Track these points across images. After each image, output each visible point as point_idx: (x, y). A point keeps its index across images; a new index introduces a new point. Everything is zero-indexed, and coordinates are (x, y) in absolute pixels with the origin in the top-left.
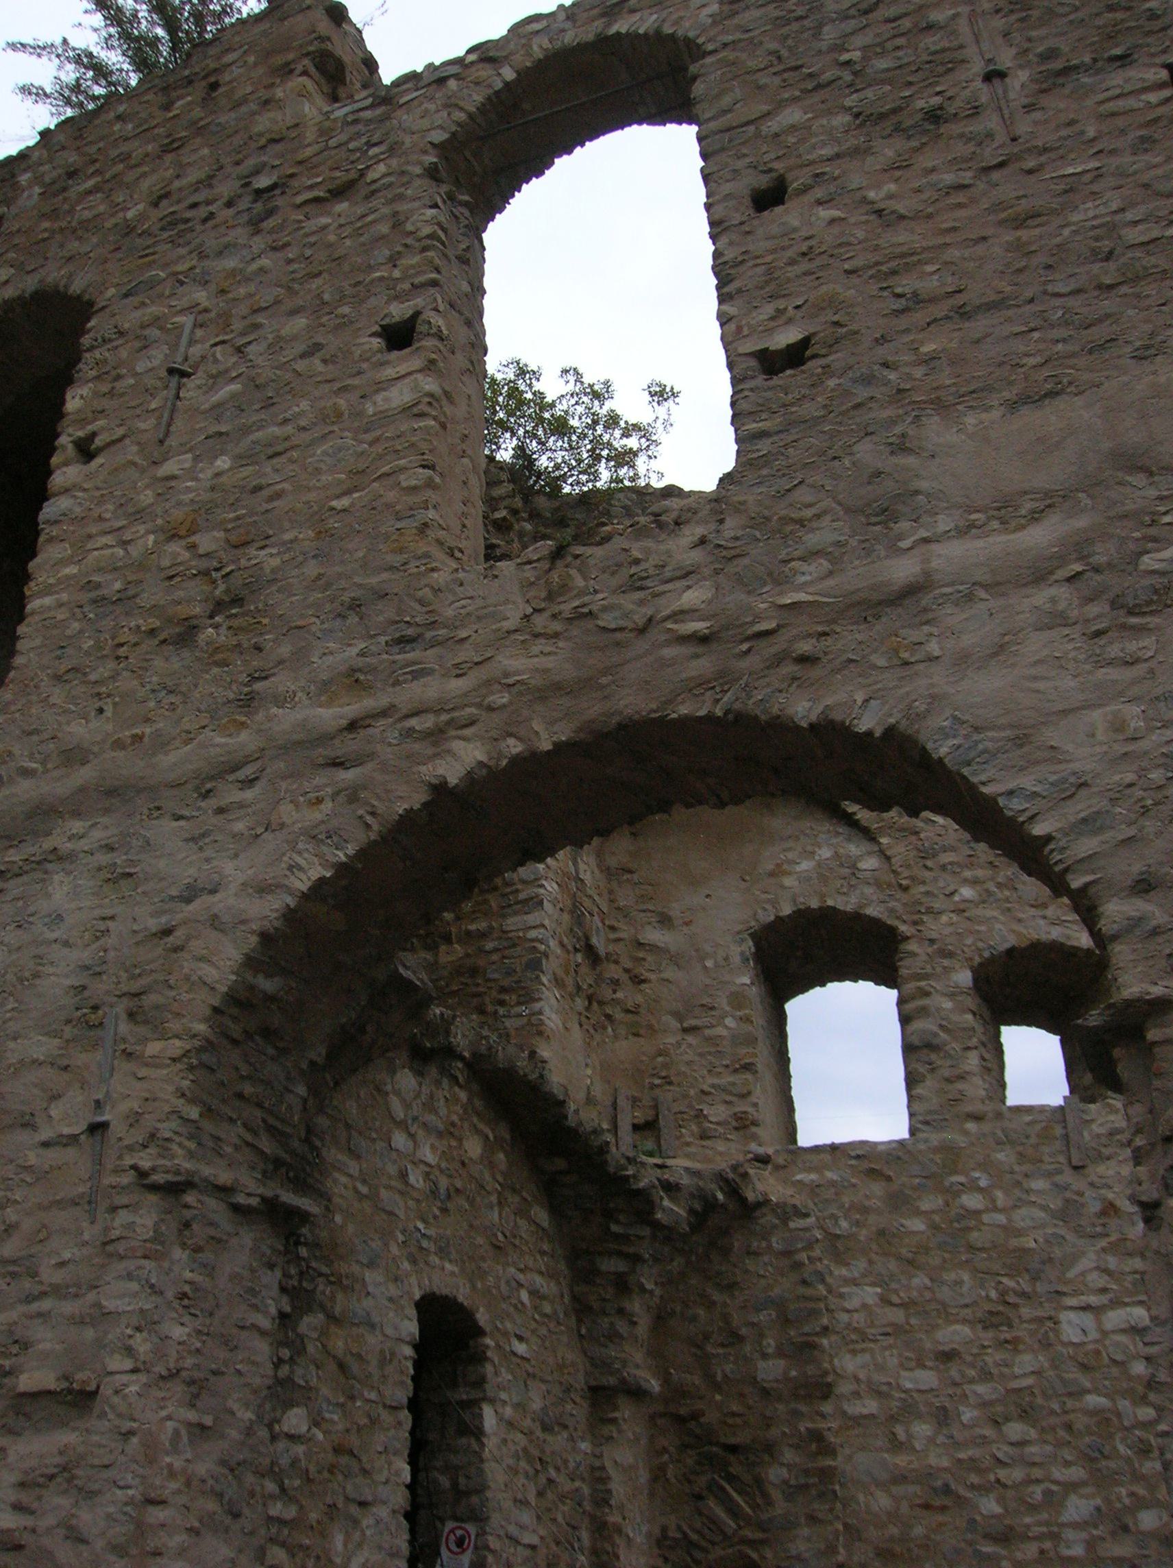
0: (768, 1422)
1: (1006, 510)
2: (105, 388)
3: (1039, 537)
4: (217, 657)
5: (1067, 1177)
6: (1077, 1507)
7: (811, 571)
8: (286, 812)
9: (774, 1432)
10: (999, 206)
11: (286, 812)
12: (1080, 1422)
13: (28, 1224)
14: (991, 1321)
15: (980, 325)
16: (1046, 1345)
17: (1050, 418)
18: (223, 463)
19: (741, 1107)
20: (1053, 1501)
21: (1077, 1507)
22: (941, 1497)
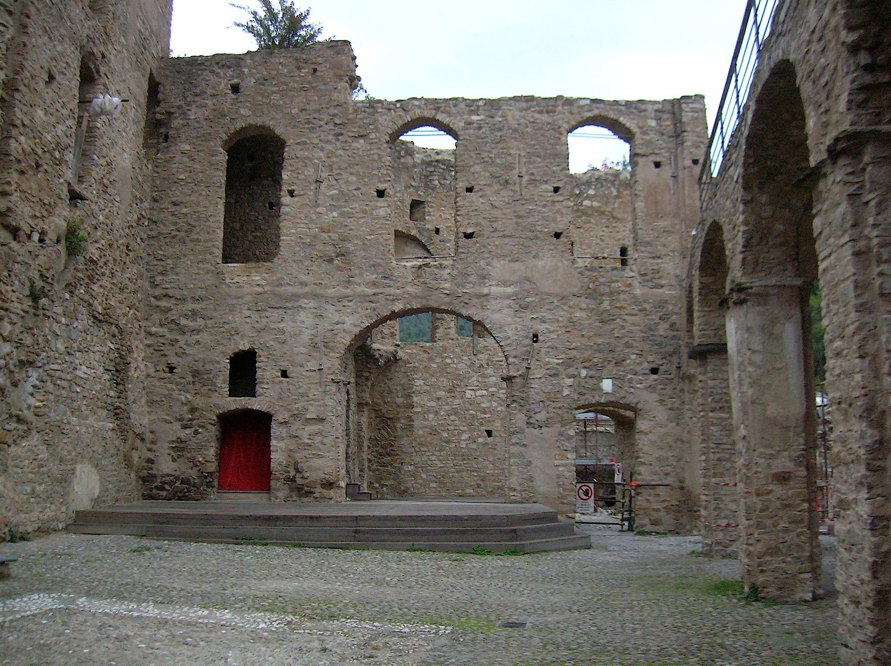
0: (398, 413)
1: (505, 283)
2: (295, 175)
3: (510, 290)
4: (339, 269)
5: (472, 357)
6: (465, 436)
7: (469, 286)
8: (359, 310)
9: (399, 416)
10: (515, 212)
11: (359, 310)
12: (468, 417)
13: (305, 386)
14: (450, 391)
15: (507, 240)
16: (462, 398)
17: (516, 266)
18: (335, 214)
19: (392, 330)
20: (460, 434)
21: (465, 436)
22: (434, 432)
